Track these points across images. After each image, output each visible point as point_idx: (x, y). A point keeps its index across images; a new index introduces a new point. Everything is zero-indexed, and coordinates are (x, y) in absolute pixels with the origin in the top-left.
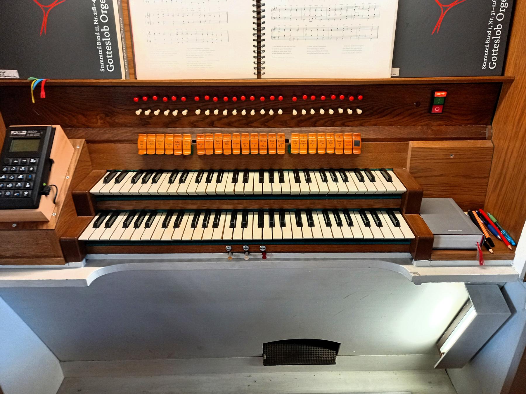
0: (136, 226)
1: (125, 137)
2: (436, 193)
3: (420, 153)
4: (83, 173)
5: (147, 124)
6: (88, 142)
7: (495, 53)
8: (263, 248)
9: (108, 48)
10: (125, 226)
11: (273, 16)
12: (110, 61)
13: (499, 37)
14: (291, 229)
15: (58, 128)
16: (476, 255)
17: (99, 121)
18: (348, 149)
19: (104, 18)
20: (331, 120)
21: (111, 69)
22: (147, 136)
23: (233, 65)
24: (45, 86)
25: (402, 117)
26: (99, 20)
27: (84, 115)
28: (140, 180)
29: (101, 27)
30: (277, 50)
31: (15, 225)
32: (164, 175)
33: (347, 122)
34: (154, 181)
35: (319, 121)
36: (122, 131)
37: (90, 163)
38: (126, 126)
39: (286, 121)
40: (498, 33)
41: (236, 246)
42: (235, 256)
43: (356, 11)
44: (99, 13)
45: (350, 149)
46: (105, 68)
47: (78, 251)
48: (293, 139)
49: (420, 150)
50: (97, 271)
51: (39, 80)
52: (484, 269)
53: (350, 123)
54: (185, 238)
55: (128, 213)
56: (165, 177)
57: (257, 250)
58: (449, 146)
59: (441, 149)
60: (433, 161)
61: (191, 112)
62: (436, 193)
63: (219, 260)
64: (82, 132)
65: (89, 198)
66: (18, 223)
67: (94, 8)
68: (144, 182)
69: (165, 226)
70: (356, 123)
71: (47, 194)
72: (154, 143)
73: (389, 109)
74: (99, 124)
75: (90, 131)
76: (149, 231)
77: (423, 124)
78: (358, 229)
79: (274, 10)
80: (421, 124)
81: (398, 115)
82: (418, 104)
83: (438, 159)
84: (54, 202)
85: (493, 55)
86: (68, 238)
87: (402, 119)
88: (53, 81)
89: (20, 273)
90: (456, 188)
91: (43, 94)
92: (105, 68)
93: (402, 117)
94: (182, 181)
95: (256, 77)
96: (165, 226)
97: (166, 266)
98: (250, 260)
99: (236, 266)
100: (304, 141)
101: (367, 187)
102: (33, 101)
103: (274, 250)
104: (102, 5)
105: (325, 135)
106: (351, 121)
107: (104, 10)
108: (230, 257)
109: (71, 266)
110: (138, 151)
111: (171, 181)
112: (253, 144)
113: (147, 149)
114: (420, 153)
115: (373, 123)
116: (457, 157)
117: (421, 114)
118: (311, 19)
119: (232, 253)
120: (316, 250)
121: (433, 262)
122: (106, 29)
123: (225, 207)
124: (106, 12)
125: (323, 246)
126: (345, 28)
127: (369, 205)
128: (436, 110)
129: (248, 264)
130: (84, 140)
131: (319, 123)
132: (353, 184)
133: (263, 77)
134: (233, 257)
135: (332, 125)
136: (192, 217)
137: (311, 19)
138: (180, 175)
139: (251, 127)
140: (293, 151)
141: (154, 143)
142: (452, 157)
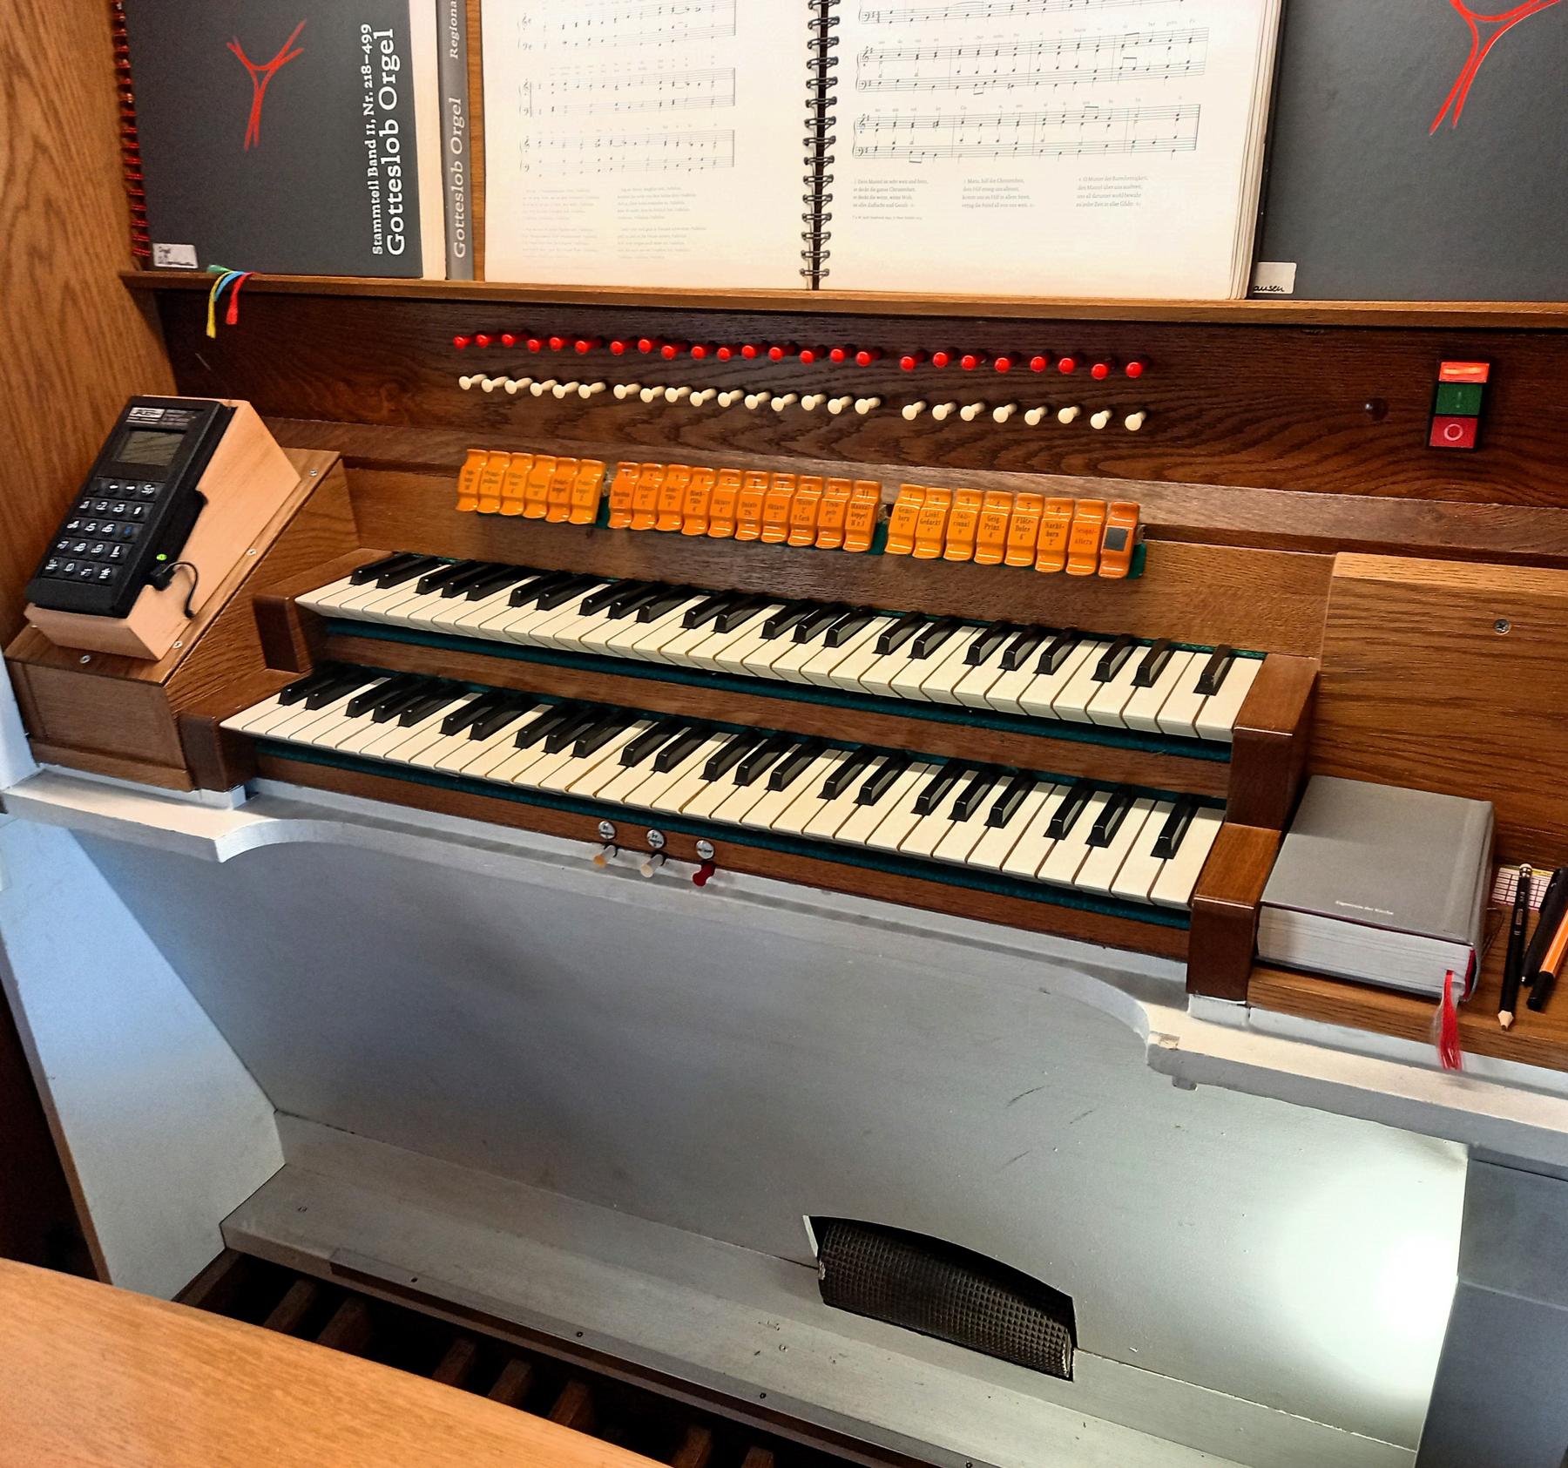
0: (961, 813)
1: (442, 456)
2: (1428, 770)
3: (1366, 603)
4: (299, 548)
5: (498, 423)
6: (349, 462)
7: (396, 206)
8: (704, 848)
9: (395, 186)
10: (924, 807)
11: (862, 79)
12: (397, 225)
13: (397, 159)
14: (801, 805)
15: (244, 409)
16: (1430, 1020)
17: (386, 404)
18: (1081, 556)
19: (388, 98)
20: (1049, 448)
21: (396, 246)
22: (743, 479)
23: (737, 247)
24: (240, 293)
25: (1314, 457)
26: (376, 102)
27: (348, 382)
28: (908, 646)
29: (381, 126)
30: (869, 194)
31: (86, 659)
32: (1081, 650)
33: (1106, 459)
34: (1046, 667)
35: (1005, 448)
36: (438, 439)
37: (352, 527)
38: (450, 424)
39: (897, 441)
40: (393, 145)
41: (630, 824)
42: (624, 859)
43: (1128, 52)
44: (378, 84)
45: (1089, 556)
46: (384, 245)
47: (249, 765)
48: (906, 501)
49: (1397, 593)
50: (258, 826)
51: (234, 274)
52: (1463, 1086)
53: (1121, 466)
54: (1124, 887)
55: (847, 755)
56: (1087, 656)
57: (687, 852)
58: (1492, 587)
59: (1476, 599)
60: (1418, 640)
61: (890, 404)
62: (1428, 770)
63: (575, 862)
64: (343, 433)
65: (292, 618)
66: (94, 654)
67: (366, 69)
68: (1009, 663)
69: (1057, 831)
70: (1141, 465)
71: (161, 585)
72: (508, 483)
73: (1259, 420)
74: (385, 413)
75: (361, 431)
76: (1000, 838)
77: (1403, 488)
78: (1024, 840)
79: (865, 56)
80: (1396, 488)
81: (1297, 447)
82: (1380, 410)
83: (1440, 634)
84: (188, 613)
85: (392, 211)
86: (197, 716)
87: (1318, 462)
88: (271, 278)
89: (86, 793)
90: (1521, 765)
91: (232, 315)
92: (384, 245)
93: (1314, 457)
94: (1144, 678)
95: (804, 283)
96: (1057, 831)
97: (433, 851)
98: (656, 879)
99: (621, 891)
100: (940, 514)
101: (901, 673)
102: (211, 331)
103: (740, 863)
104: (384, 59)
105: (1012, 500)
106: (1121, 458)
107: (389, 73)
108: (599, 859)
109: (205, 800)
110: (457, 503)
111: (1104, 673)
112: (771, 507)
113: (1005, 548)
114: (1366, 603)
115: (1203, 470)
116: (1528, 636)
117: (1393, 450)
118: (980, 84)
119: (617, 847)
120: (869, 889)
121: (1260, 1016)
122: (390, 128)
123: (1153, 778)
124: (393, 79)
125: (893, 879)
126: (1090, 114)
127: (1107, 769)
128: (1451, 436)
129: (651, 892)
130: (337, 454)
131: (1006, 456)
132: (1074, 687)
133: (823, 283)
134: (612, 861)
135: (1055, 467)
136: (1160, 819)
137: (980, 85)
138: (1140, 654)
139: (790, 452)
140: (895, 546)
141: (1034, 527)
142: (1505, 632)
